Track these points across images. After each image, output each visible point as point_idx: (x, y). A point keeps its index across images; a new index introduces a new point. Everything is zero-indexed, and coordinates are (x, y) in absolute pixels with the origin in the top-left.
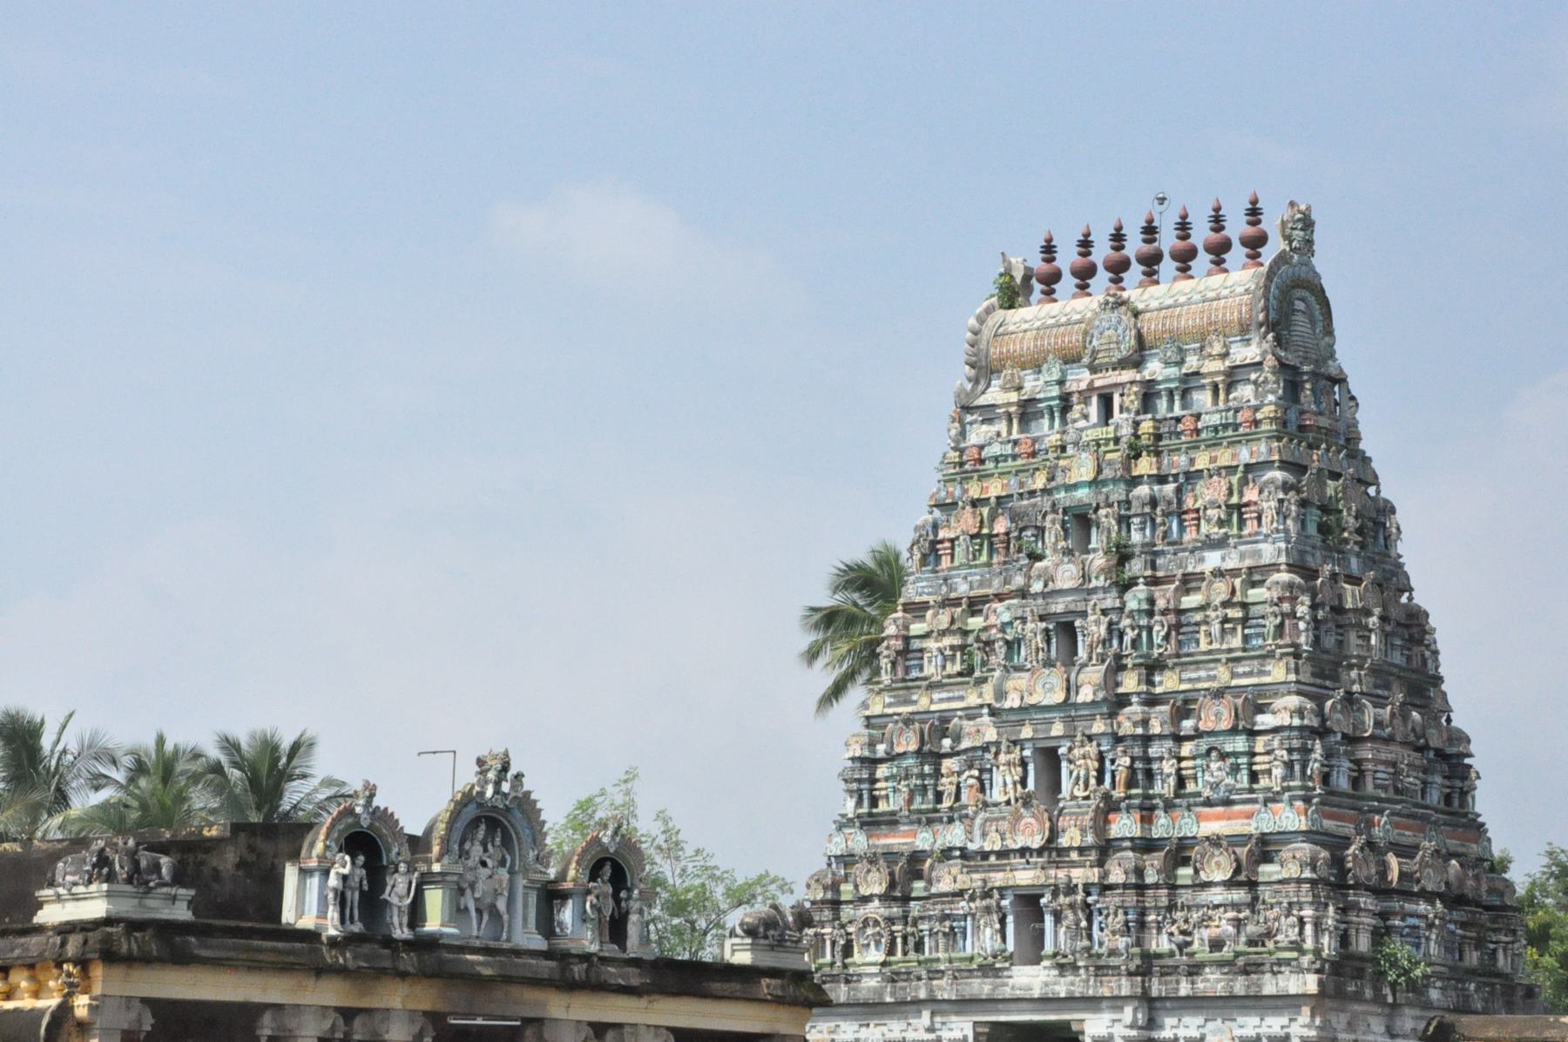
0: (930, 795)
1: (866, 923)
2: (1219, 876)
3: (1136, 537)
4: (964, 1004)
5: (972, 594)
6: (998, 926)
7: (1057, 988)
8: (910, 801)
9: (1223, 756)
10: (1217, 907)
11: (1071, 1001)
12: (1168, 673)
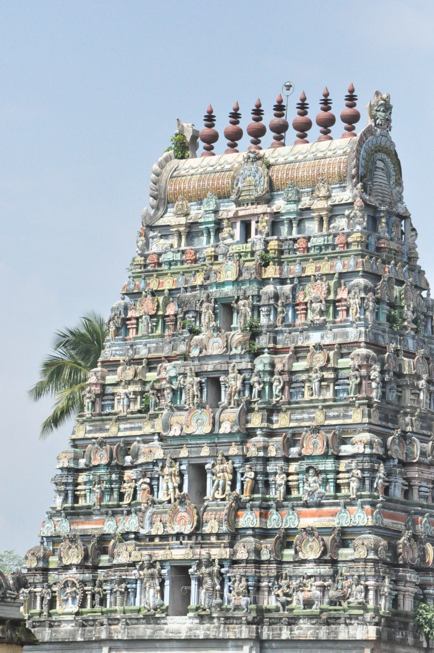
0: (115, 495)
1: (66, 585)
3: (264, 321)
5: (150, 356)
6: (158, 588)
7: (198, 632)
8: (101, 499)
9: (318, 473)
10: (310, 577)
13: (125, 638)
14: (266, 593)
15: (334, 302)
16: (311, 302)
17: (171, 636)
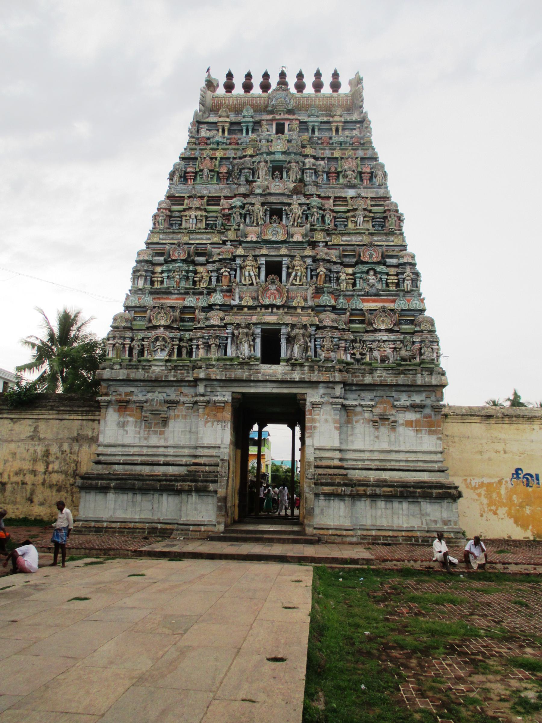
0: (191, 281)
1: (157, 339)
5: (210, 195)
7: (293, 376)
10: (384, 341)
13: (224, 378)
14: (342, 352)
15: (361, 173)
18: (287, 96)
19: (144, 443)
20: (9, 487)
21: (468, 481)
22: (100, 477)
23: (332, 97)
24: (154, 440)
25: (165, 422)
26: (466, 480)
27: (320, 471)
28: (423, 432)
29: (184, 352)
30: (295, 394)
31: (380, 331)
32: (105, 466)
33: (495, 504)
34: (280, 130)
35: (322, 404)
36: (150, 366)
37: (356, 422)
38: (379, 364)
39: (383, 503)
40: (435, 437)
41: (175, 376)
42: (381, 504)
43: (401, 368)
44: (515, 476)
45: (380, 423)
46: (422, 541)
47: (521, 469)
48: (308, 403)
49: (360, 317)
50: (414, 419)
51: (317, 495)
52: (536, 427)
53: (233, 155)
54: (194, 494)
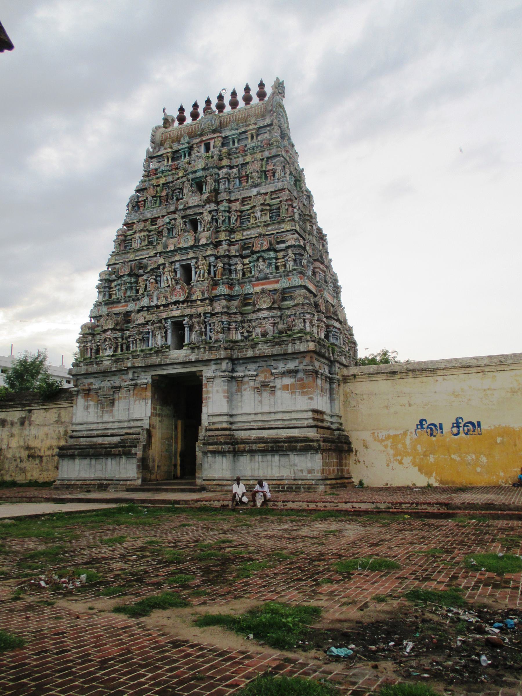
0: (134, 291)
1: (105, 340)
2: (264, 306)
3: (222, 187)
4: (147, 368)
6: (164, 334)
7: (191, 357)
8: (125, 293)
10: (264, 318)
11: (197, 362)
12: (237, 233)
14: (234, 332)
15: (265, 172)
16: (251, 173)
17: (173, 361)
18: (212, 118)
19: (100, 420)
20: (44, 458)
21: (376, 434)
22: (70, 448)
23: (245, 109)
24: (107, 418)
25: (112, 403)
26: (374, 433)
27: (210, 433)
28: (297, 394)
29: (125, 347)
30: (195, 372)
31: (263, 310)
32: (75, 439)
33: (400, 455)
34: (207, 149)
35: (214, 378)
36: (102, 361)
37: (245, 390)
38: (260, 339)
39: (260, 457)
40: (306, 397)
41: (116, 367)
42: (258, 458)
43: (276, 340)
44: (419, 427)
45: (263, 389)
46: (287, 488)
47: (425, 420)
48: (204, 379)
49: (246, 300)
50: (289, 383)
51: (205, 453)
52: (440, 378)
53: (171, 180)
54: (123, 457)
